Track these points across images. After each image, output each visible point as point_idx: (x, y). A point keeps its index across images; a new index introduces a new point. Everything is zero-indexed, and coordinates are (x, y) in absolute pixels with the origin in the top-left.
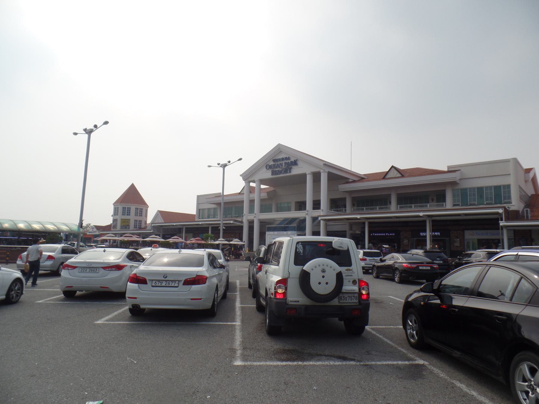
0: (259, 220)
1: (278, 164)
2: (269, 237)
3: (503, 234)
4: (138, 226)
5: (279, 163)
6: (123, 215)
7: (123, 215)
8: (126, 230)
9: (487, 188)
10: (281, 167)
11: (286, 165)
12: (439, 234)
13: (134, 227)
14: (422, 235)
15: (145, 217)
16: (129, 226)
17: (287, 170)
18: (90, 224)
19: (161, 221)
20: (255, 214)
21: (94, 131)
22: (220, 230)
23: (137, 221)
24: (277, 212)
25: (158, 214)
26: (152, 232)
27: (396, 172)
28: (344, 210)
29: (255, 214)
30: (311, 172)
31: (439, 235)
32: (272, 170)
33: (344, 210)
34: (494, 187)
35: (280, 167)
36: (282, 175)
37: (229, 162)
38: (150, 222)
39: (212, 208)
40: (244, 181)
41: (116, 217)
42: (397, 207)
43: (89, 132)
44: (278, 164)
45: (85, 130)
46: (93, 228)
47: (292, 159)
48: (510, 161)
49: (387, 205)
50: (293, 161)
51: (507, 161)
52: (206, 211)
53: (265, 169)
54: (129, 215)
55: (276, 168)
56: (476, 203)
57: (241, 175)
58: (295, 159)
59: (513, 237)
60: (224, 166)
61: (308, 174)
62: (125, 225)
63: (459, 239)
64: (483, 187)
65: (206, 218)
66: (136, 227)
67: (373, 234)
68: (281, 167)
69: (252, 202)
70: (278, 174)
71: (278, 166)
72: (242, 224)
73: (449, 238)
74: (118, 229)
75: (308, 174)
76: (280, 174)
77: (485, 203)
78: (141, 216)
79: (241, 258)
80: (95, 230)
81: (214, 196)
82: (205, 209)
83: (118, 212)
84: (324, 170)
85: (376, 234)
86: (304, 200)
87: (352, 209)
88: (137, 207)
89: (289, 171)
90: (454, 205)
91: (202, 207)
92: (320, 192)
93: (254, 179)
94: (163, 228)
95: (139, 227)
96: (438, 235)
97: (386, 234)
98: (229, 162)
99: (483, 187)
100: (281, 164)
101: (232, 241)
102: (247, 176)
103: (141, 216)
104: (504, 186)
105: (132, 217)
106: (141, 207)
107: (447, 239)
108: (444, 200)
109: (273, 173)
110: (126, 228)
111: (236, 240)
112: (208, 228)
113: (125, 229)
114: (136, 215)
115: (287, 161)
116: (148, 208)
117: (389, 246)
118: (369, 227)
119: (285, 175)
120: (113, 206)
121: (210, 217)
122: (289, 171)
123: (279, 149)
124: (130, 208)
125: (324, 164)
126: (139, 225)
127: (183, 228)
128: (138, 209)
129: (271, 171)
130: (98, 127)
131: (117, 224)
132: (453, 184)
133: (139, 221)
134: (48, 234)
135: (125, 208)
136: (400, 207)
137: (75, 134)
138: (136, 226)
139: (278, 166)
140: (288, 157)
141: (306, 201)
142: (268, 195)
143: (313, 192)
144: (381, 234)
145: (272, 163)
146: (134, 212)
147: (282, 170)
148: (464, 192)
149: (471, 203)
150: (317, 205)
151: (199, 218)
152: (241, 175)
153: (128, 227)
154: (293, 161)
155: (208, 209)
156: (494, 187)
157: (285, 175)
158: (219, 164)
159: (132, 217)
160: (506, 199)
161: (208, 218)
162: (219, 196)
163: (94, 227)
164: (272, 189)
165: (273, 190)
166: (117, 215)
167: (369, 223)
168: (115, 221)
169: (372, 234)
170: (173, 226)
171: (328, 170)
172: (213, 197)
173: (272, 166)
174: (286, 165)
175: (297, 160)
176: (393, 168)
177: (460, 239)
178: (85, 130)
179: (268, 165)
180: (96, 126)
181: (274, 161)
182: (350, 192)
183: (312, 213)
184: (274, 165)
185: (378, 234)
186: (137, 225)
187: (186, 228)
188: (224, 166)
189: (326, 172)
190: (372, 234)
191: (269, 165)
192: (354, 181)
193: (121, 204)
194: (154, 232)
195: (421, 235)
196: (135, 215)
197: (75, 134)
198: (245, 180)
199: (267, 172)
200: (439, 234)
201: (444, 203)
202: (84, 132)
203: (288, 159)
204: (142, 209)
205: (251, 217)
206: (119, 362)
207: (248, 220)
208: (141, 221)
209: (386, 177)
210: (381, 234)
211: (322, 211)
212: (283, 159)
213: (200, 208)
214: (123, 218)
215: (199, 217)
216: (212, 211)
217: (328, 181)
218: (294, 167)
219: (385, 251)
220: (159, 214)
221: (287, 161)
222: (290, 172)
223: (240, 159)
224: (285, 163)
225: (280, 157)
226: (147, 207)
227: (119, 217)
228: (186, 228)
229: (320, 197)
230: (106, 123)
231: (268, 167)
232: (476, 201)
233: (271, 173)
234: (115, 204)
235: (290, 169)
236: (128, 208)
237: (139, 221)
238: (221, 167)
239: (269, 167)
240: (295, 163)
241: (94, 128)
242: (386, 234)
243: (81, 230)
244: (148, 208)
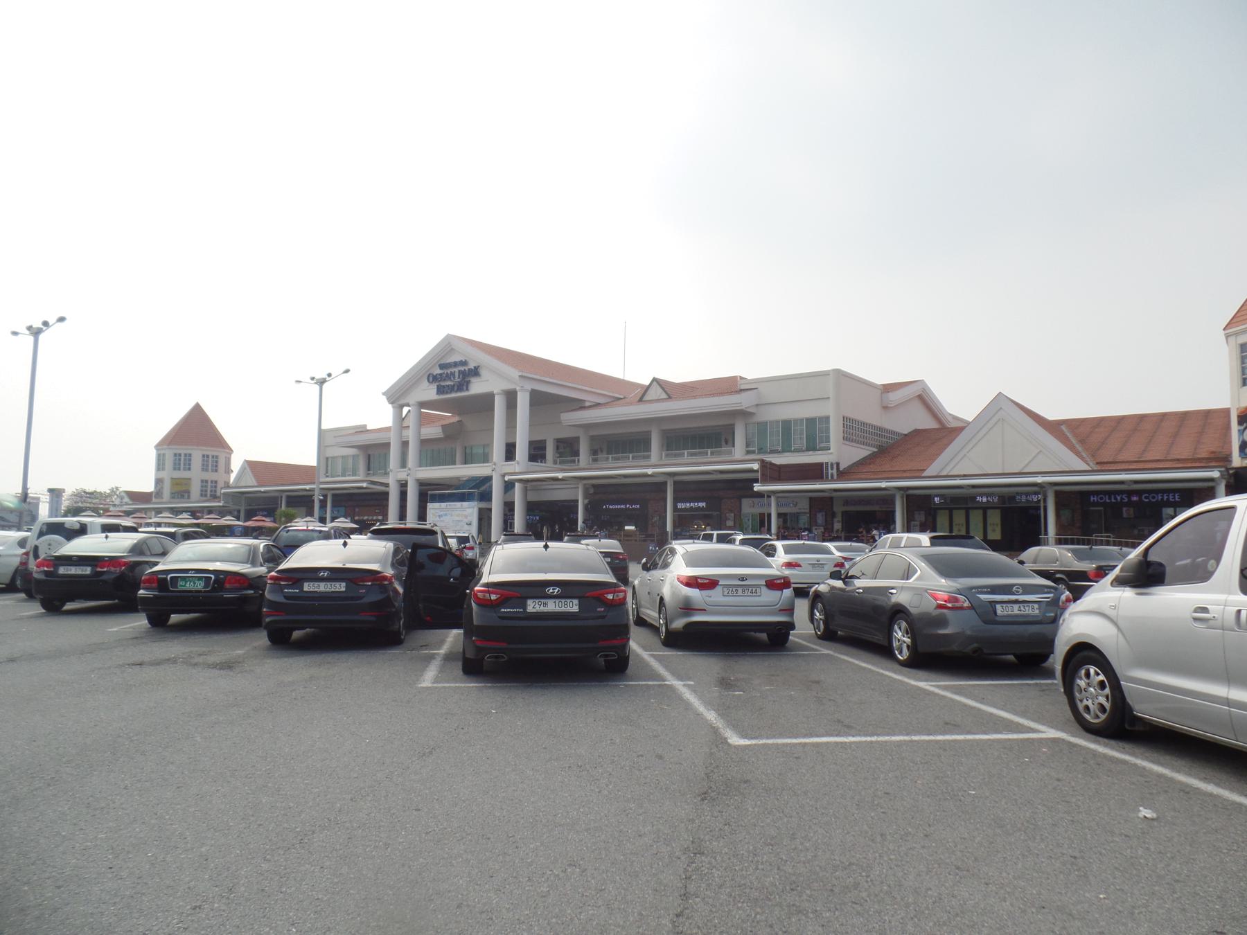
0: (418, 480)
1: (447, 373)
3: (770, 505)
4: (209, 493)
5: (449, 372)
6: (175, 469)
7: (175, 469)
8: (183, 500)
9: (796, 421)
10: (452, 379)
11: (461, 376)
13: (202, 495)
15: (225, 473)
16: (188, 492)
17: (463, 385)
18: (117, 488)
19: (251, 484)
20: (410, 469)
21: (44, 331)
22: (314, 501)
23: (207, 481)
24: (465, 464)
25: (245, 469)
26: (221, 504)
27: (660, 390)
28: (686, 453)
29: (495, 464)
30: (502, 390)
32: (437, 384)
33: (686, 453)
35: (451, 380)
36: (453, 395)
37: (329, 375)
39: (350, 456)
40: (390, 405)
41: (164, 474)
42: (662, 454)
43: (36, 333)
44: (447, 373)
45: (29, 328)
46: (122, 498)
47: (472, 366)
48: (829, 375)
50: (473, 368)
51: (824, 374)
52: (340, 461)
53: (426, 383)
54: (189, 469)
55: (445, 380)
56: (780, 449)
57: (384, 394)
58: (476, 365)
59: (808, 511)
60: (322, 382)
61: (498, 394)
62: (181, 489)
63: (733, 515)
64: (816, 419)
65: (338, 476)
66: (206, 496)
68: (452, 379)
69: (405, 444)
70: (447, 393)
71: (448, 377)
72: (387, 489)
73: (718, 513)
74: (164, 500)
75: (498, 394)
76: (451, 392)
77: (793, 449)
78: (216, 471)
80: (126, 500)
82: (337, 457)
83: (164, 464)
84: (522, 387)
85: (611, 507)
87: (663, 455)
88: (206, 453)
89: (465, 388)
90: (748, 452)
91: (331, 453)
92: (493, 429)
94: (246, 497)
95: (211, 495)
98: (329, 375)
99: (816, 419)
100: (453, 374)
101: (202, 518)
102: (396, 396)
103: (216, 471)
104: (821, 418)
105: (196, 474)
106: (215, 454)
108: (577, 454)
109: (440, 390)
110: (183, 497)
111: (342, 519)
112: (665, 483)
113: (181, 498)
114: (205, 468)
115: (462, 368)
116: (230, 454)
117: (636, 527)
118: (675, 491)
120: (155, 451)
121: (347, 474)
122: (465, 388)
123: (449, 344)
124: (190, 455)
125: (520, 376)
126: (211, 491)
127: (281, 497)
128: (208, 456)
129: (436, 387)
130: (50, 324)
131: (162, 488)
132: (743, 414)
133: (212, 482)
135: (180, 455)
136: (667, 456)
137: (15, 333)
138: (204, 493)
139: (448, 377)
141: (515, 443)
142: (444, 431)
143: (530, 426)
144: (619, 507)
145: (438, 371)
146: (193, 462)
147: (454, 385)
148: (763, 426)
149: (773, 448)
150: (510, 453)
151: (327, 476)
152: (384, 394)
153: (186, 495)
154: (473, 368)
155: (343, 457)
158: (313, 379)
159: (196, 474)
161: (343, 475)
162: (362, 432)
163: (123, 494)
164: (456, 419)
165: (458, 421)
166: (163, 469)
167: (675, 483)
168: (159, 482)
170: (646, 475)
171: (529, 386)
172: (350, 434)
174: (461, 376)
175: (479, 366)
177: (735, 515)
178: (29, 328)
180: (46, 324)
181: (442, 366)
182: (587, 427)
183: (504, 467)
184: (441, 374)
186: (206, 491)
187: (288, 497)
188: (322, 382)
189: (526, 391)
191: (433, 375)
192: (597, 405)
193: (170, 447)
194: (225, 505)
196: (203, 470)
197: (15, 333)
198: (392, 403)
199: (430, 387)
201: (576, 458)
202: (28, 332)
203: (464, 363)
204: (217, 457)
205: (402, 475)
206: (574, 930)
207: (399, 481)
208: (216, 482)
210: (619, 507)
211: (518, 463)
212: (455, 364)
213: (327, 456)
214: (174, 477)
215: (327, 473)
216: (350, 461)
217: (531, 405)
218: (473, 380)
220: (248, 469)
222: (467, 390)
223: (347, 371)
224: (459, 371)
225: (451, 359)
226: (230, 451)
227: (166, 475)
228: (288, 497)
230: (62, 319)
231: (431, 379)
233: (436, 390)
234: (159, 446)
235: (468, 383)
236: (185, 455)
237: (212, 482)
238: (316, 383)
239: (433, 379)
240: (475, 372)
241: (42, 327)
243: (25, 506)
244: (232, 455)
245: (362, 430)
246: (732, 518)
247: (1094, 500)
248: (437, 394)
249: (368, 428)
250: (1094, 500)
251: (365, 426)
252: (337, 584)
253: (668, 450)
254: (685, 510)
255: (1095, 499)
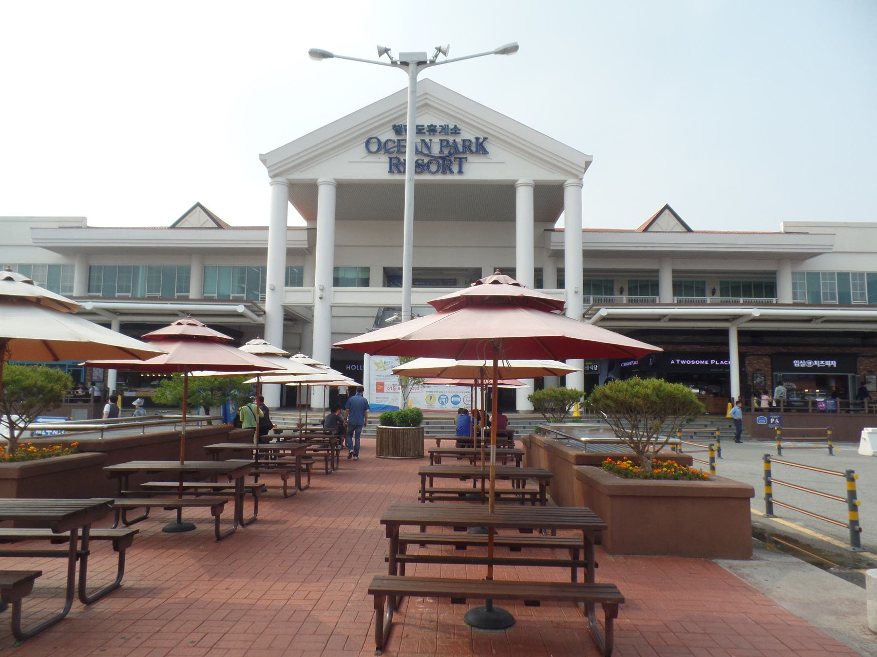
2: (376, 364)
12: (834, 363)
14: (799, 366)
31: (835, 366)
34: (867, 274)
38: (232, 226)
40: (269, 179)
47: (467, 134)
49: (613, 294)
50: (474, 140)
57: (264, 159)
63: (875, 377)
67: (676, 362)
79: (328, 439)
81: (56, 225)
85: (683, 362)
86: (399, 266)
93: (314, 177)
96: (832, 366)
97: (709, 362)
107: (850, 375)
119: (439, 177)
134: (640, 477)
140: (451, 127)
144: (698, 362)
148: (814, 277)
152: (264, 159)
156: (867, 274)
157: (439, 177)
158: (383, 51)
160: (828, 300)
162: (80, 227)
169: (673, 362)
173: (390, 145)
176: (667, 211)
179: (374, 140)
185: (688, 362)
190: (673, 362)
195: (796, 365)
200: (834, 363)
209: (648, 230)
210: (698, 362)
219: (824, 405)
221: (451, 139)
229: (514, 258)
231: (374, 147)
232: (835, 300)
240: (480, 148)
242: (709, 362)
245: (79, 224)
246: (874, 381)
247: (348, 366)
248: (391, 171)
249: (89, 224)
250: (348, 366)
251: (84, 219)
252: (562, 536)
253: (629, 295)
254: (806, 369)
255: (349, 367)
